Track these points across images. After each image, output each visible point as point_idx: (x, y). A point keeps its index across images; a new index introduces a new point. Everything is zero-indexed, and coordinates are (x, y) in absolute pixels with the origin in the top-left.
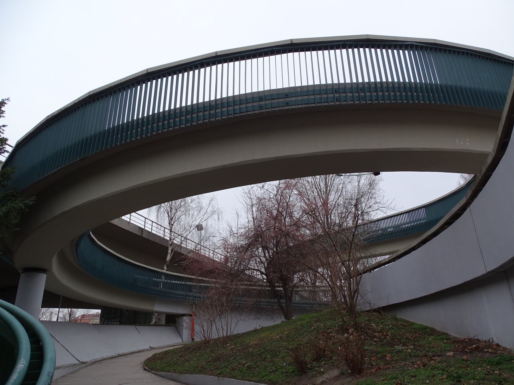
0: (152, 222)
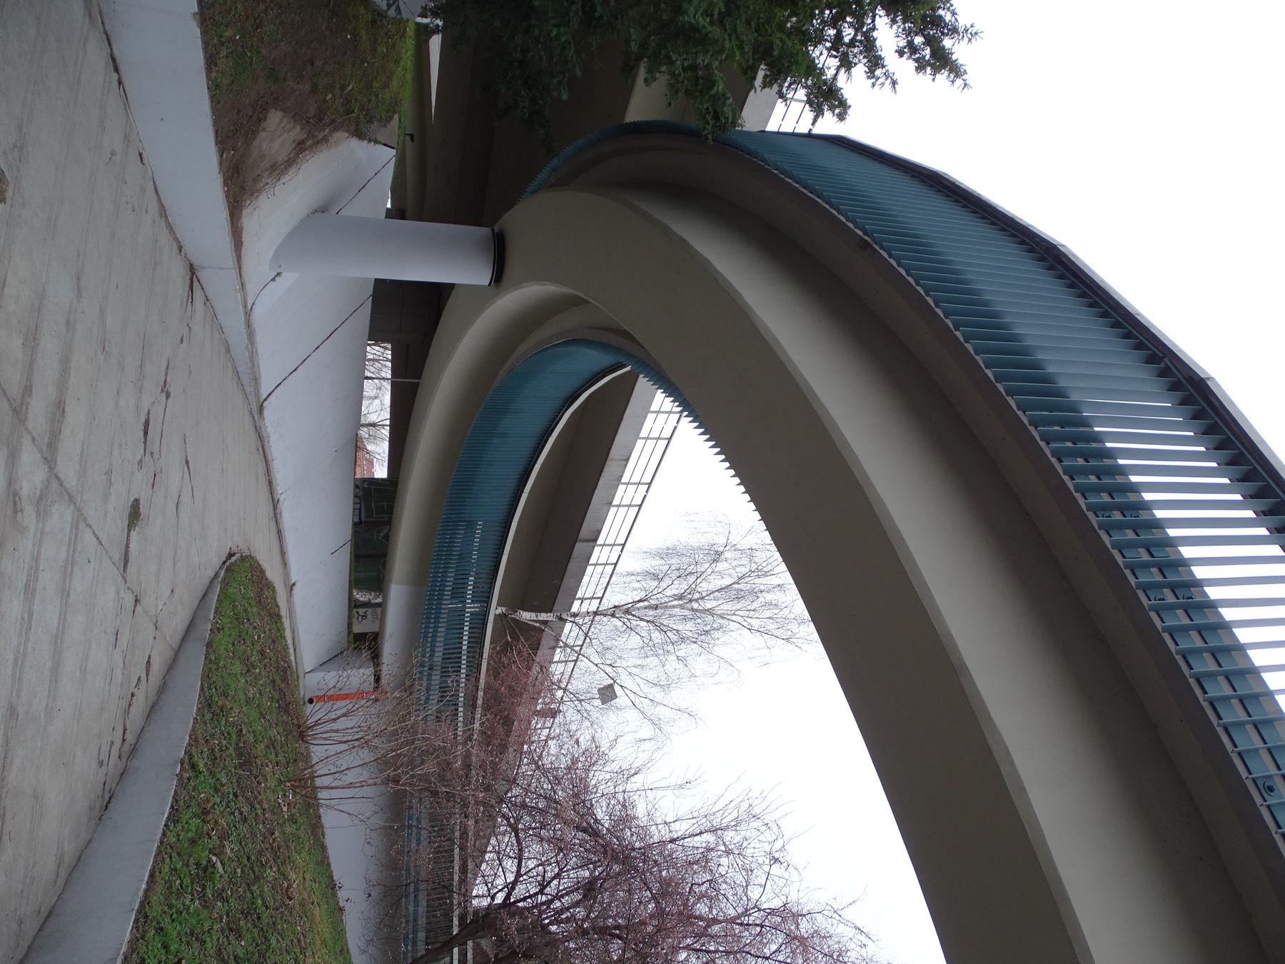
0: (616, 564)
